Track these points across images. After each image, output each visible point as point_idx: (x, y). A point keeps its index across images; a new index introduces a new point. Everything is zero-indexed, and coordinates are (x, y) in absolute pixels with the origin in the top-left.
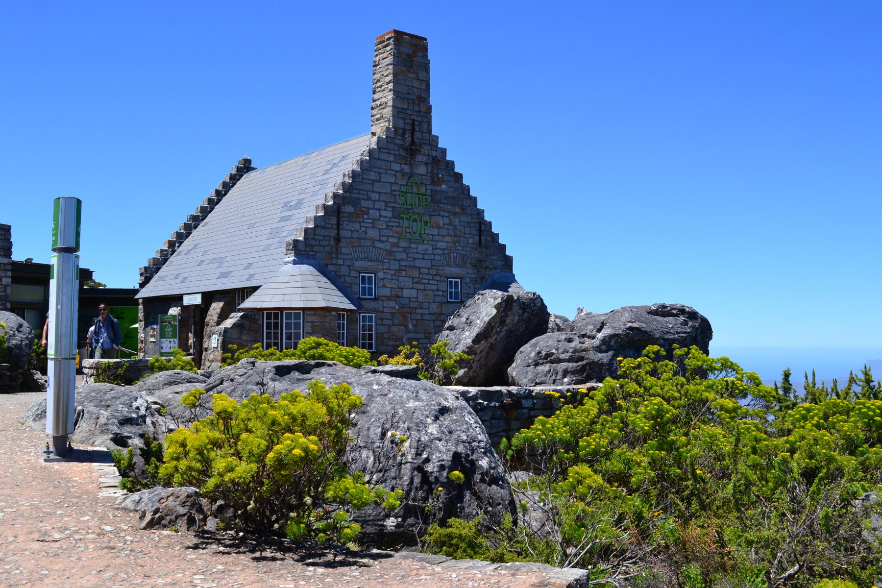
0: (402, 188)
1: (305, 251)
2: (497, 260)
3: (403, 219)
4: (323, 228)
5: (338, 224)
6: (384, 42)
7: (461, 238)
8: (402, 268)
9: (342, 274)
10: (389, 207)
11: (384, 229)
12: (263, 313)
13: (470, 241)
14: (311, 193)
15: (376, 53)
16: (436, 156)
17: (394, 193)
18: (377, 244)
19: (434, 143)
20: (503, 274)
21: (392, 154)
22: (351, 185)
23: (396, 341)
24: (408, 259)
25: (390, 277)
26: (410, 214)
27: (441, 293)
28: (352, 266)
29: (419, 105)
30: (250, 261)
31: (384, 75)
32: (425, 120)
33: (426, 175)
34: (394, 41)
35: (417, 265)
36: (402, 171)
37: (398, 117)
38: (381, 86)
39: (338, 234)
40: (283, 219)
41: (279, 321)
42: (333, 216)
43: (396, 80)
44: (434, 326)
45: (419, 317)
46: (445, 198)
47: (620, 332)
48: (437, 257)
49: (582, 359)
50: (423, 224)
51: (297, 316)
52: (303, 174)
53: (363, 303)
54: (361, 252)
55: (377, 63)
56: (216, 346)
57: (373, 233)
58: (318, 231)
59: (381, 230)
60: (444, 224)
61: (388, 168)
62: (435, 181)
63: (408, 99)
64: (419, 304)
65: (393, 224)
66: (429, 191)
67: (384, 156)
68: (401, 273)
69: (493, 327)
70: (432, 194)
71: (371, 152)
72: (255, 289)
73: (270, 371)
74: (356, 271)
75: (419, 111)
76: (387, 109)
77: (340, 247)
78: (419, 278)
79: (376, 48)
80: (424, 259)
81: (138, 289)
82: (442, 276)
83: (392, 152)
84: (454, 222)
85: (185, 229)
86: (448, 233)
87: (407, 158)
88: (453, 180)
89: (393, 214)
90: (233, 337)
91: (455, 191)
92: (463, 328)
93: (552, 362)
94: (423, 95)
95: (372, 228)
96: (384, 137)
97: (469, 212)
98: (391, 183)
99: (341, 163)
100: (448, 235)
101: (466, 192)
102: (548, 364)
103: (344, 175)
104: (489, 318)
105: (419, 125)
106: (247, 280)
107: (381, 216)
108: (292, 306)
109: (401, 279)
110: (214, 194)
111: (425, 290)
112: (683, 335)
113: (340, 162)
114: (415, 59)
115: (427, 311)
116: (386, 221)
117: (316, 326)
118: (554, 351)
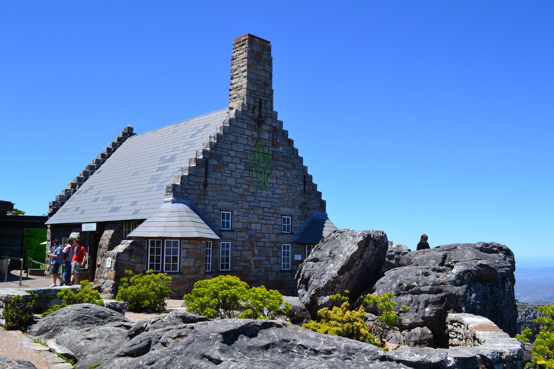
0: (252, 148)
1: (181, 193)
2: (316, 203)
3: (252, 171)
4: (195, 176)
5: (206, 173)
6: (240, 42)
7: (292, 187)
8: (251, 207)
9: (208, 211)
10: (243, 162)
11: (240, 178)
12: (148, 241)
13: (298, 189)
14: (182, 151)
15: (234, 50)
16: (276, 127)
17: (246, 152)
18: (234, 189)
19: (274, 117)
20: (319, 213)
21: (246, 123)
22: (216, 144)
23: (246, 263)
24: (256, 201)
25: (242, 214)
26: (258, 168)
27: (277, 227)
28: (216, 205)
29: (265, 89)
30: (135, 200)
31: (240, 66)
32: (269, 100)
33: (269, 140)
34: (248, 42)
35: (261, 206)
36: (252, 135)
37: (250, 96)
38: (237, 74)
39: (206, 181)
40: (160, 169)
41: (161, 247)
42: (202, 167)
43: (249, 70)
44: (273, 251)
45: (262, 244)
46: (282, 157)
47: (473, 268)
48: (275, 200)
49: (441, 291)
50: (266, 175)
51: (175, 244)
52: (174, 137)
53: (223, 233)
54: (222, 195)
55: (235, 57)
56: (110, 267)
57: (231, 181)
58: (192, 178)
59: (237, 179)
60: (280, 176)
61: (243, 133)
62: (275, 144)
63: (258, 84)
64: (262, 235)
65: (245, 175)
66: (270, 151)
67: (239, 124)
68: (250, 211)
69: (355, 261)
70: (273, 153)
71: (231, 121)
72: (141, 221)
73: (216, 338)
74: (218, 209)
75: (264, 93)
76: (242, 90)
77: (207, 191)
78: (263, 215)
79: (234, 47)
80: (266, 201)
81: (47, 217)
82: (279, 214)
83: (245, 121)
84: (287, 175)
85: (84, 175)
86: (283, 183)
87: (255, 127)
88: (287, 144)
89: (245, 167)
90: (124, 259)
91: (288, 153)
92: (327, 260)
93: (413, 293)
94: (268, 82)
95: (230, 177)
96: (241, 110)
97: (297, 168)
98: (244, 144)
99: (205, 130)
100: (284, 184)
101: (295, 154)
102: (409, 295)
103: (211, 137)
104: (351, 253)
105: (264, 103)
106: (133, 214)
107: (237, 168)
108: (172, 236)
109: (250, 216)
110: (106, 151)
111: (266, 224)
112: (507, 269)
113: (203, 128)
114: (263, 56)
115: (267, 240)
116: (240, 173)
117: (190, 252)
118: (415, 284)
